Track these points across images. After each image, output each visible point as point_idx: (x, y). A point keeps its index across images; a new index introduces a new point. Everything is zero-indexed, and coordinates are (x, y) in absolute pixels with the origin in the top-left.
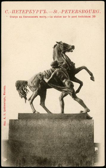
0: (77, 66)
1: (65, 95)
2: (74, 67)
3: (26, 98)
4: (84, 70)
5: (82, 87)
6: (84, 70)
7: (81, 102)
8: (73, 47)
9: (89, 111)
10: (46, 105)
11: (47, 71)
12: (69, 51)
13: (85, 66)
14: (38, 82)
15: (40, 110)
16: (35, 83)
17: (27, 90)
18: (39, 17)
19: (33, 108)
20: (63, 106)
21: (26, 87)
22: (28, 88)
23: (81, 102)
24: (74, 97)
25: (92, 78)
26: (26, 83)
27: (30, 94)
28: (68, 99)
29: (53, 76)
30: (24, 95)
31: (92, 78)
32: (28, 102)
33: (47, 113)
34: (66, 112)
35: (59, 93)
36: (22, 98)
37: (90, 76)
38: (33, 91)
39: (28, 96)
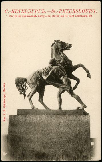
1: (63, 92)
2: (71, 64)
3: (25, 95)
4: (81, 68)
5: (79, 84)
6: (81, 67)
7: (78, 99)
8: (70, 46)
9: (85, 107)
11: (45, 69)
12: (66, 49)
14: (36, 79)
15: (39, 106)
16: (33, 80)
17: (26, 87)
19: (32, 104)
20: (60, 102)
21: (25, 84)
22: (27, 85)
23: (78, 99)
24: (71, 93)
25: (89, 76)
26: (25, 80)
27: (29, 90)
28: (66, 95)
30: (23, 91)
31: (89, 76)
32: (27, 99)
34: (63, 108)
35: (57, 90)
36: (21, 94)
37: (87, 74)
38: (32, 87)
39: (27, 93)
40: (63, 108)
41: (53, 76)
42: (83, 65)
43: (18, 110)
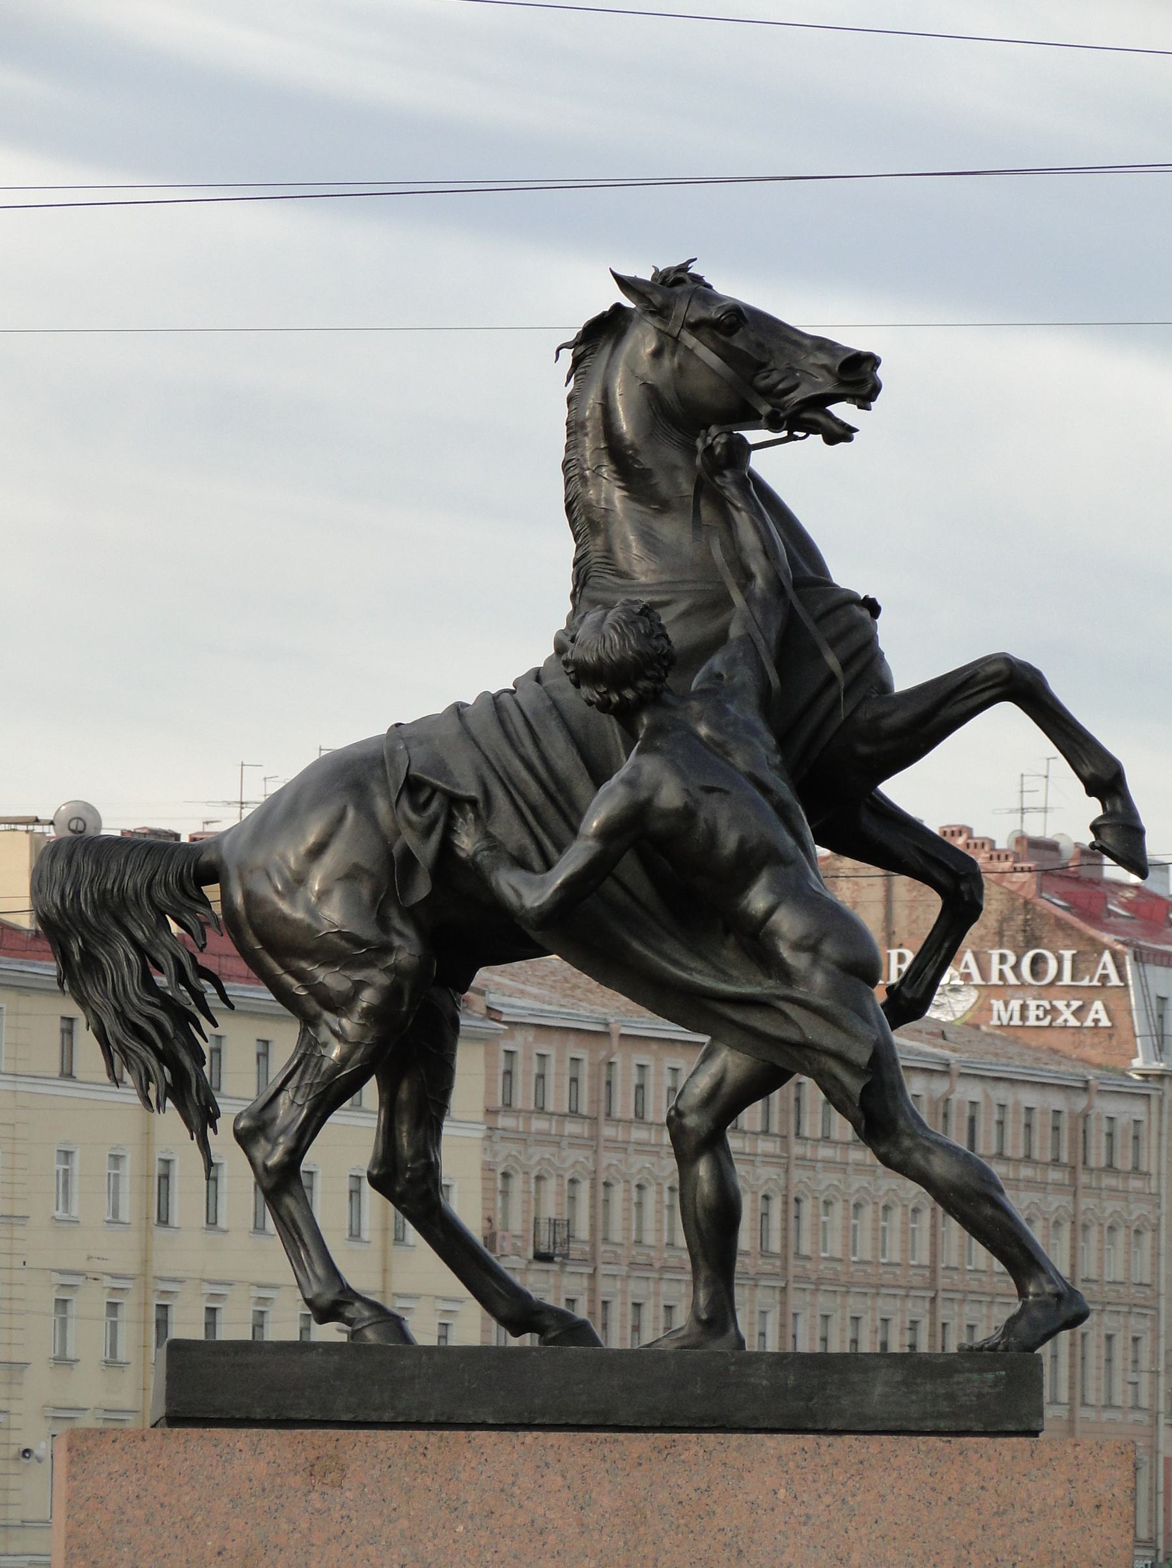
1: (761, 1084)
2: (866, 659)
3: (201, 1115)
5: (1064, 689)
6: (1005, 721)
8: (858, 376)
9: (1066, 1312)
11: (496, 733)
12: (807, 418)
14: (374, 899)
16: (337, 897)
18: (615, 1040)
20: (714, 1234)
23: (974, 1203)
24: (878, 1114)
27: (250, 1048)
28: (795, 1148)
29: (607, 834)
30: (165, 1057)
33: (374, 1079)
34: (759, 1323)
35: (676, 1064)
37: (1094, 808)
39: (237, 1089)
40: (947, 1351)
41: (75, 949)
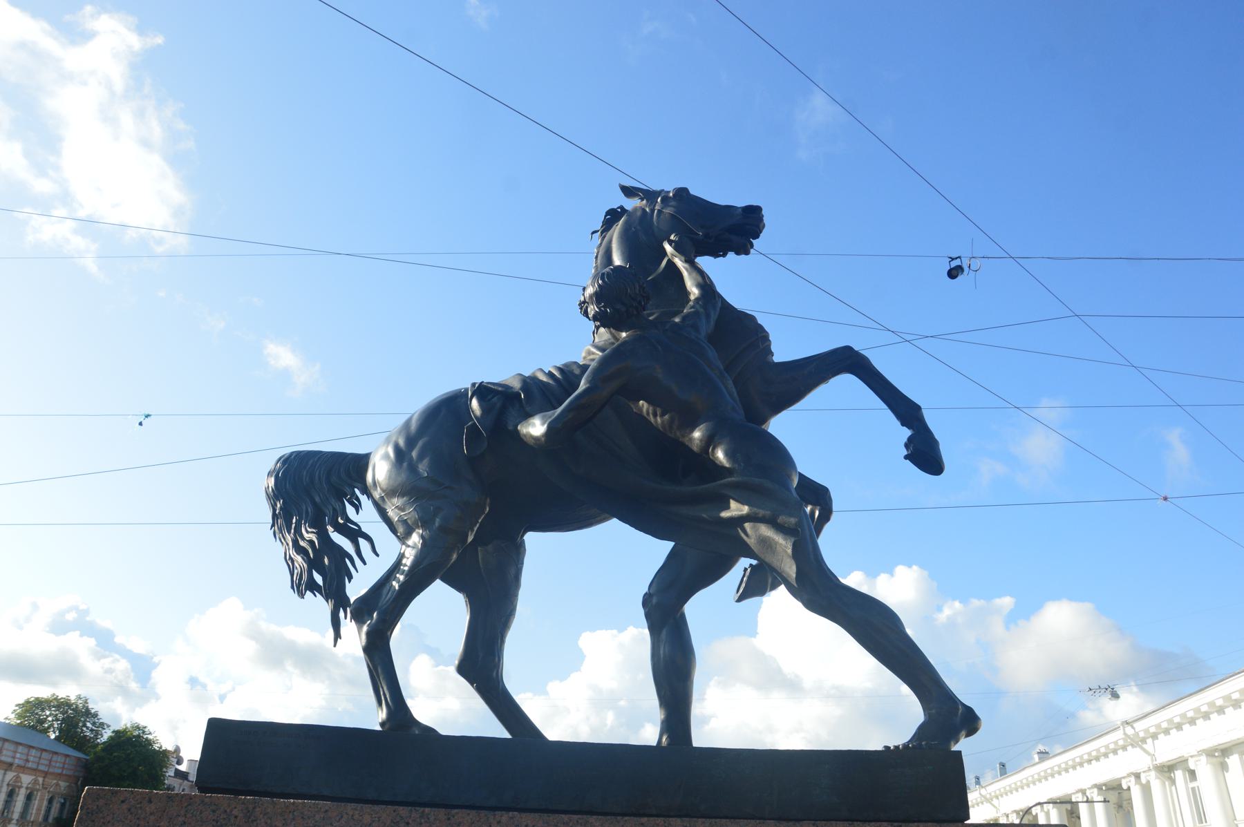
0: (786, 347)
4: (846, 385)
5: (880, 362)
7: (875, 628)
10: (398, 639)
13: (834, 517)
15: (445, 704)
17: (355, 534)
19: (384, 689)
21: (357, 508)
22: (366, 516)
23: (875, 628)
25: (925, 454)
26: (346, 472)
30: (323, 572)
31: (925, 454)
32: (354, 636)
36: (302, 595)
37: (906, 433)
38: (401, 530)
42: (828, 520)
43: (158, 698)
